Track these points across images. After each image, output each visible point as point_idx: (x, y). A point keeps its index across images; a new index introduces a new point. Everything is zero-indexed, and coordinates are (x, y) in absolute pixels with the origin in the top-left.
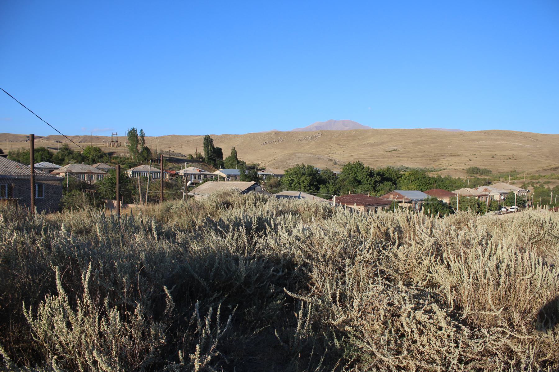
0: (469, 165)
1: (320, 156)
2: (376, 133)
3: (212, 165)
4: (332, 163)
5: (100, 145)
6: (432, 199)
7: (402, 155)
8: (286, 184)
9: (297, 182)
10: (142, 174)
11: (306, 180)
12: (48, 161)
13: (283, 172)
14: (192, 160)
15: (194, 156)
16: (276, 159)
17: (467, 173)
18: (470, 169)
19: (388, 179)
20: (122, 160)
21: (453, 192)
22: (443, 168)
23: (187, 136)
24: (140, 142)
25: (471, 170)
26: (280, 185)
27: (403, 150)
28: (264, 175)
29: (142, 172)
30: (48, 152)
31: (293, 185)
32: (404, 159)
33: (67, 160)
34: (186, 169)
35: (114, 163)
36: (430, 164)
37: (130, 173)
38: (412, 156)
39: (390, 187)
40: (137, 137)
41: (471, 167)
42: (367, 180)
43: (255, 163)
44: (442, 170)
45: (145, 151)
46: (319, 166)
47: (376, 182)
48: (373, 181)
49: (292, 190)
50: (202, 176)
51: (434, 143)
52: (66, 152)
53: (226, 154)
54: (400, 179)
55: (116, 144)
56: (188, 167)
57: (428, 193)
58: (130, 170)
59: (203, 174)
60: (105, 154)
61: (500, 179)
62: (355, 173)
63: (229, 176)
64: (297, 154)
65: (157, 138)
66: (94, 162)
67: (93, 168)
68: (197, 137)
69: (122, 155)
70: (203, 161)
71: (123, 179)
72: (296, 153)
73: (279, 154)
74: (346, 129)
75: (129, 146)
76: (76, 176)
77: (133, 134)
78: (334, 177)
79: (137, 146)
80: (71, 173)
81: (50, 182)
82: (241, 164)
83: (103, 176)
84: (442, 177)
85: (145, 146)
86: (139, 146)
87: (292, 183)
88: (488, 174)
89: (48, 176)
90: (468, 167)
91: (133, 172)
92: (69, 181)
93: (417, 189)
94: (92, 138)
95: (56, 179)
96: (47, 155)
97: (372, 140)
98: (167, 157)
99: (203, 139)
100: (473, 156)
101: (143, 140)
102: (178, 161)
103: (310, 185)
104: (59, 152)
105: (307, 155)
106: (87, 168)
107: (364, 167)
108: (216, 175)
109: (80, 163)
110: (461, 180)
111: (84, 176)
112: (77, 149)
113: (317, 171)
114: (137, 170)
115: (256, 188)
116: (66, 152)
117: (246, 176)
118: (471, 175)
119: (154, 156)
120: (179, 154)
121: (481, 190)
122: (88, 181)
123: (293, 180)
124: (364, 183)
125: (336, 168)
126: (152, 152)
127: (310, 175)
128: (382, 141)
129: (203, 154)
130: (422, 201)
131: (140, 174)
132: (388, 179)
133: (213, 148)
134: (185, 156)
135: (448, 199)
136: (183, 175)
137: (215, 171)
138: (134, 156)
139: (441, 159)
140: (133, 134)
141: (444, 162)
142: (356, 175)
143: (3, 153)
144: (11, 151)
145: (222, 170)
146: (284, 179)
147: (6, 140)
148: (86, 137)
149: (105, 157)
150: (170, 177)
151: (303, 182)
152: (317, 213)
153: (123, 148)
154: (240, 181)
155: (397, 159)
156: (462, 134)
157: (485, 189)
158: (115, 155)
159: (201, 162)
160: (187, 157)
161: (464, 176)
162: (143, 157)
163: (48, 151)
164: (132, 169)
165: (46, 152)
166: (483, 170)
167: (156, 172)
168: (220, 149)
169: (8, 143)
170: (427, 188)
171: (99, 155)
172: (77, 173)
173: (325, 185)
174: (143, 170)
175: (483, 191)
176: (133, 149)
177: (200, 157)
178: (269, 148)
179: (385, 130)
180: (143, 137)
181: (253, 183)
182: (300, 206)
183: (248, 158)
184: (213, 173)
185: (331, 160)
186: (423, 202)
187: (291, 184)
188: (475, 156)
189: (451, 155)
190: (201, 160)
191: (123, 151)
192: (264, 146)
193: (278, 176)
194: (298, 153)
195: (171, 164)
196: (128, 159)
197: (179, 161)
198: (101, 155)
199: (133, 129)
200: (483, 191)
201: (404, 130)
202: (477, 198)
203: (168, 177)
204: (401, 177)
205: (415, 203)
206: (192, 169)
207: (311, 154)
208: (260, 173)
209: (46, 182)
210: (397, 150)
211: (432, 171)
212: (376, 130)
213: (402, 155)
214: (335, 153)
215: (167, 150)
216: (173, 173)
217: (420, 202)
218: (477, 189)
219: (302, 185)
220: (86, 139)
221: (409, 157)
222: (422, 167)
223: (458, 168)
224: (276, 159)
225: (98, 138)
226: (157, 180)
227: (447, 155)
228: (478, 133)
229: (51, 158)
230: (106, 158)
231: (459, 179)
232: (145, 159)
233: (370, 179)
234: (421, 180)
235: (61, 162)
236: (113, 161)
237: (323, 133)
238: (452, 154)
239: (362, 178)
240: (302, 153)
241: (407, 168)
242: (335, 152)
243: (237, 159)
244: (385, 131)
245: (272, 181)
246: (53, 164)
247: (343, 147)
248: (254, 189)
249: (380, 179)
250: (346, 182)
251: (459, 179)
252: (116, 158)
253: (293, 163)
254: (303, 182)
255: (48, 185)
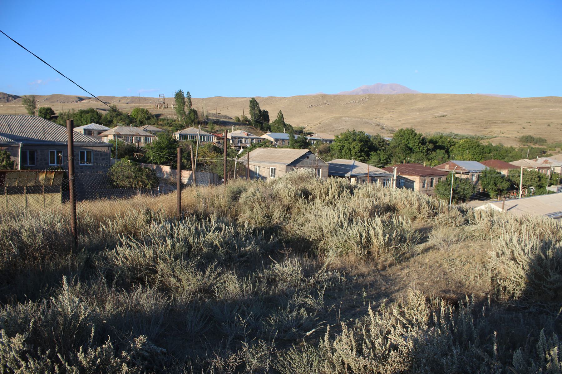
0: (522, 133)
1: (367, 120)
2: (426, 97)
3: (259, 128)
4: (379, 128)
5: (147, 106)
6: (490, 172)
7: (451, 121)
8: (336, 150)
9: (347, 149)
10: (190, 137)
11: (357, 146)
12: (98, 123)
13: (332, 137)
14: (241, 123)
15: (241, 119)
16: (322, 122)
17: (520, 141)
18: (523, 137)
19: (441, 148)
20: (169, 122)
21: (511, 163)
22: (494, 136)
23: (233, 98)
24: (187, 103)
25: (524, 139)
26: (329, 150)
27: (453, 116)
28: (312, 140)
29: (190, 135)
30: (97, 114)
31: (343, 151)
32: (454, 126)
33: (115, 122)
34: (233, 132)
35: (161, 125)
36: (481, 131)
37: (177, 135)
38: (462, 122)
39: (443, 155)
40: (184, 99)
41: (525, 135)
42: (419, 148)
43: (301, 126)
44: (493, 138)
45: (193, 113)
46: (369, 131)
47: (428, 150)
48: (425, 149)
49: (341, 158)
50: (249, 140)
51: (485, 109)
52: (114, 114)
53: (273, 118)
54: (452, 147)
55: (163, 106)
56: (235, 130)
57: (485, 164)
58: (177, 132)
59: (250, 138)
60: (153, 116)
61: (556, 149)
62: (407, 140)
63: (277, 140)
64: (344, 118)
65: (203, 99)
66: (142, 123)
67: (140, 130)
68: (243, 99)
69: (170, 117)
70: (250, 124)
71: (172, 144)
72: (343, 116)
73: (326, 117)
74: (394, 93)
75: (176, 108)
76: (124, 140)
77: (179, 96)
78: (384, 143)
79: (184, 108)
80: (119, 136)
81: (99, 149)
82: (288, 128)
83: (151, 139)
84: (494, 145)
85: (192, 108)
86: (186, 108)
87: (342, 149)
88: (542, 143)
89: (96, 143)
90: (521, 135)
91: (181, 135)
92: (118, 144)
93: (472, 159)
94: (140, 100)
95: (104, 145)
96: (96, 116)
97: (420, 105)
98: (214, 120)
99: (249, 102)
100: (527, 124)
101: (190, 102)
102: (224, 124)
103: (361, 151)
104: (108, 114)
105: (353, 119)
106: (135, 130)
107: (416, 134)
108: (264, 139)
109: (128, 125)
110: (514, 148)
111: (132, 138)
112: (125, 111)
113: (368, 137)
114: (185, 133)
115: (310, 156)
116: (114, 114)
117: (296, 141)
118: (524, 143)
119: (201, 119)
120: (226, 117)
121: (540, 161)
122: (136, 143)
123: (343, 146)
124: (416, 151)
125: (383, 133)
126: (199, 114)
127: (361, 141)
128: (431, 106)
129: (249, 117)
130: (480, 172)
131: (187, 136)
132: (441, 148)
133: (260, 111)
134: (231, 118)
135: (507, 171)
136: (230, 138)
137: (263, 134)
138: (181, 118)
139: (493, 127)
140: (179, 96)
141: (496, 129)
142: (408, 142)
143: (55, 114)
144: (62, 112)
145: (269, 133)
146: (333, 143)
147: (58, 101)
148: (133, 97)
149: (152, 119)
150: (218, 141)
151: (354, 148)
152: (419, 210)
153: (170, 110)
154: (290, 148)
155: (447, 125)
156: (517, 101)
157: (545, 161)
158: (162, 117)
159: (248, 125)
160: (234, 120)
161: (517, 145)
162: (190, 119)
163: (97, 112)
164: (179, 132)
165: (95, 113)
166: (538, 138)
167: (203, 135)
168: (267, 112)
169: (59, 104)
170: (482, 158)
171: (146, 117)
172: (126, 135)
173: (377, 152)
174: (190, 133)
175: (543, 163)
176: (181, 112)
177: (246, 120)
178: (315, 112)
179: (434, 95)
180: (189, 98)
181: (307, 150)
182: (399, 201)
183: (293, 121)
184: (261, 137)
185: (378, 125)
186: (481, 173)
187: (341, 150)
188: (530, 124)
189: (504, 122)
190: (247, 123)
191: (171, 113)
192: (310, 109)
193: (326, 141)
194: (345, 117)
195: (218, 126)
196: (175, 121)
197: (225, 123)
198: (148, 117)
199: (180, 91)
200: (543, 163)
201: (455, 95)
202: (537, 170)
203: (215, 140)
204: (454, 145)
205: (472, 175)
206: (239, 133)
207: (358, 118)
208: (308, 137)
209: (94, 148)
210: (446, 116)
211: (482, 139)
212: (426, 95)
213: (451, 121)
214: (383, 117)
215: (214, 112)
216: (220, 136)
217: (477, 174)
218: (536, 160)
219: (353, 151)
220: (133, 100)
221: (459, 123)
222: (472, 134)
223: (510, 136)
224: (322, 122)
225: (145, 99)
226: (205, 143)
227: (499, 122)
228: (533, 99)
229: (100, 119)
230: (153, 120)
231: (511, 147)
232: (193, 121)
233: (422, 146)
234: (475, 149)
235: (109, 123)
236: (160, 123)
237: (370, 97)
238: (504, 121)
239: (414, 145)
240: (349, 117)
241: (456, 135)
242: (382, 116)
243: (283, 121)
244: (434, 96)
245: (321, 147)
246: (102, 126)
247: (390, 112)
248: (308, 157)
249: (433, 147)
250: (398, 150)
251: (511, 147)
252: (164, 120)
253: (339, 127)
254: (354, 148)
255: (96, 151)
